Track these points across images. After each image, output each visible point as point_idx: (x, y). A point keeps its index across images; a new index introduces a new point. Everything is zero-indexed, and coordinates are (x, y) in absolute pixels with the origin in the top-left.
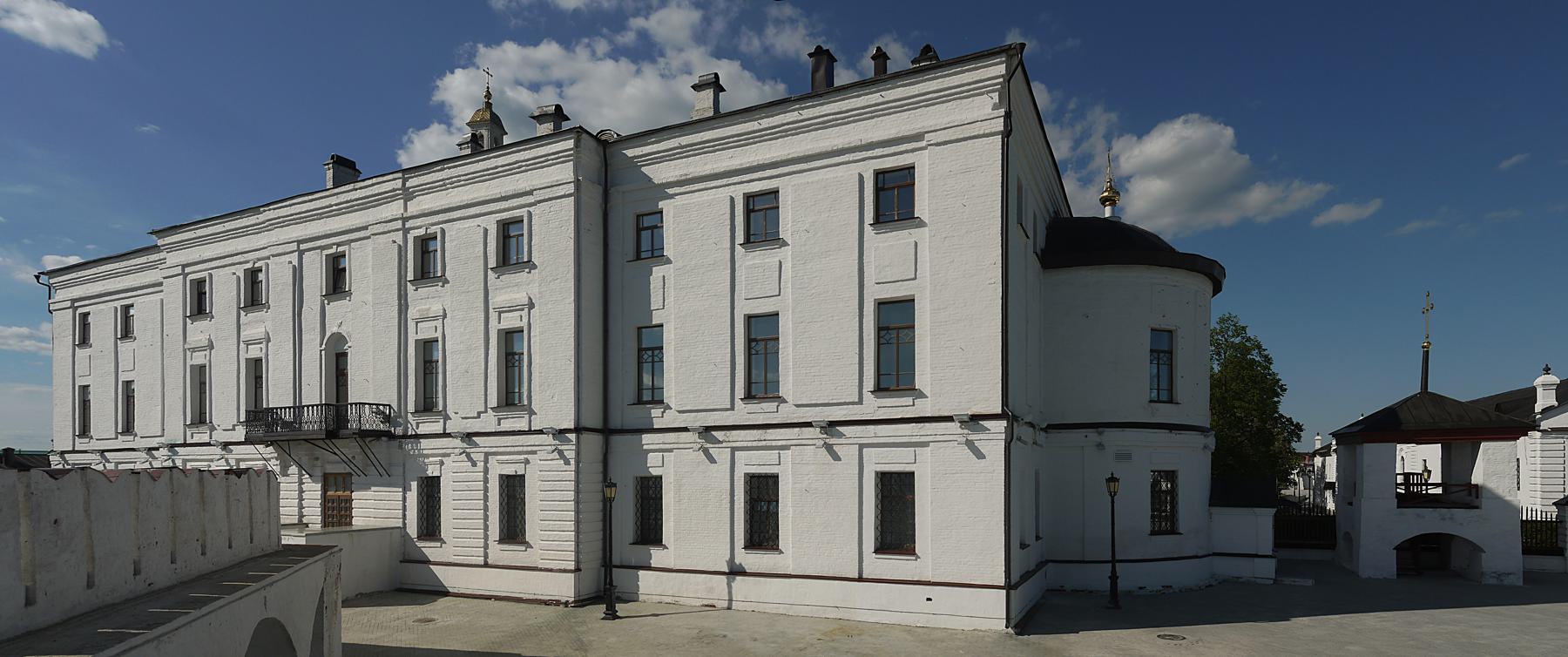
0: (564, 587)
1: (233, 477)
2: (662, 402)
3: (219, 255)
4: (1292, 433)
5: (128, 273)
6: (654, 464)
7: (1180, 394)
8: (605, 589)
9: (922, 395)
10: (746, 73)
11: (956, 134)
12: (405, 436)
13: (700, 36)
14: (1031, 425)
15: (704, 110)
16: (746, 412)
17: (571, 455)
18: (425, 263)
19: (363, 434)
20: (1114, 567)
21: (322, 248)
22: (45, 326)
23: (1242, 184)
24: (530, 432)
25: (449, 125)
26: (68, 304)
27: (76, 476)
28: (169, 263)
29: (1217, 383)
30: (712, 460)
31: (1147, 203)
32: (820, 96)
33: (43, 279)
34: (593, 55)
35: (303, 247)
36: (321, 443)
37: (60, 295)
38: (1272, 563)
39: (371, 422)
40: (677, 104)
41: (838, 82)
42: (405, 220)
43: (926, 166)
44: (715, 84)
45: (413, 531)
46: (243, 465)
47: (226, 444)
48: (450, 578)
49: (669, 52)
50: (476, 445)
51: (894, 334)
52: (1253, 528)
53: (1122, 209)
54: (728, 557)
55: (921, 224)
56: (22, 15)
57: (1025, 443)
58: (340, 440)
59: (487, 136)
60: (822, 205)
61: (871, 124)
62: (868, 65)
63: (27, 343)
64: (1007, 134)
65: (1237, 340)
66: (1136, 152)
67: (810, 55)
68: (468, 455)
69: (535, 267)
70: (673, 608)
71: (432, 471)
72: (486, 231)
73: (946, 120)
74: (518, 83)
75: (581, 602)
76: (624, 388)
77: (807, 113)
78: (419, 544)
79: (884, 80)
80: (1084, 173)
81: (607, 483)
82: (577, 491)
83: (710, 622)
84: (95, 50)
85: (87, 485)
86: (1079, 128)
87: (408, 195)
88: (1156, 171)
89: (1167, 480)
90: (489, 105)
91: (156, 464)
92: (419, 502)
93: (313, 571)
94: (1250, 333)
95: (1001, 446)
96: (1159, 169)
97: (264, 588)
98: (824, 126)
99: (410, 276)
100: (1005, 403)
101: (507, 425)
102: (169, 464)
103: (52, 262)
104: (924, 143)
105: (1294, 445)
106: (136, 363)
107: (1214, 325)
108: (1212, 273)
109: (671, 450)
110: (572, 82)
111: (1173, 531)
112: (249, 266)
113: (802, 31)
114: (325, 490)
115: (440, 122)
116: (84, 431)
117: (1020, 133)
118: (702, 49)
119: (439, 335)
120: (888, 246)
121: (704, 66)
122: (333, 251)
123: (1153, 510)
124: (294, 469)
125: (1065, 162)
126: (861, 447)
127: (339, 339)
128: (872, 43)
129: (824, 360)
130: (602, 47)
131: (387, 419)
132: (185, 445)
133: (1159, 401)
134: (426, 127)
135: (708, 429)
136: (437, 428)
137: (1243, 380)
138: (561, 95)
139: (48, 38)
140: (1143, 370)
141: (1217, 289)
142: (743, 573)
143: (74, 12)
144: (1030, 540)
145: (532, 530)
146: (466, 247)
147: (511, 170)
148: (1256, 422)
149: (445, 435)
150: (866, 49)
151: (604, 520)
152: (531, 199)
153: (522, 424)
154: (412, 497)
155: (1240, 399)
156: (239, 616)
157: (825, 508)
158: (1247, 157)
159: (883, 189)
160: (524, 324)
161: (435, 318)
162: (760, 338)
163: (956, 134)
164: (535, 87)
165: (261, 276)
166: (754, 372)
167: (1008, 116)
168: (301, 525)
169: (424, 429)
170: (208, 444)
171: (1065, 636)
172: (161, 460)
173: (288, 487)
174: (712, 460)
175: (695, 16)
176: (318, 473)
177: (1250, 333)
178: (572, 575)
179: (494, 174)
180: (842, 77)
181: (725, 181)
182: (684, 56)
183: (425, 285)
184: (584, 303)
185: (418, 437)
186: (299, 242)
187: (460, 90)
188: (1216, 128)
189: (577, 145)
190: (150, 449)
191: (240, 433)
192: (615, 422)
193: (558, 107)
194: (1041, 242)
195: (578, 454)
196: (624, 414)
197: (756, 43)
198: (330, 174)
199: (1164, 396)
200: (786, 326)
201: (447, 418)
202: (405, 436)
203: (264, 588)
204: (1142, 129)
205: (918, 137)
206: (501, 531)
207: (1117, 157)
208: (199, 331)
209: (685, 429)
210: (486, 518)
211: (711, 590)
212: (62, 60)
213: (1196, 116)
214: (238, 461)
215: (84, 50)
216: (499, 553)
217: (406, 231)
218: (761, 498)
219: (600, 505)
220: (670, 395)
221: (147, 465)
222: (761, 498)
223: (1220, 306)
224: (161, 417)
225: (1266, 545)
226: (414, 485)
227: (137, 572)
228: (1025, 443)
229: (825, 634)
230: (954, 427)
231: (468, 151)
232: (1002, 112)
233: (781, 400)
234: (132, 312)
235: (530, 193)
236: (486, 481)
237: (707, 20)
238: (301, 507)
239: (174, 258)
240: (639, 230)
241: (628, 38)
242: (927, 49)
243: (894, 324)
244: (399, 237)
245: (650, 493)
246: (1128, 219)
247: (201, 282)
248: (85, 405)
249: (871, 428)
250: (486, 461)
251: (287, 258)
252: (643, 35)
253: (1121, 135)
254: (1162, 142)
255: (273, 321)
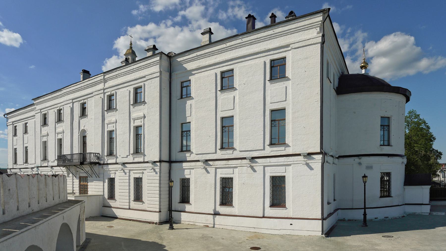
0: (155, 218)
1: (54, 177)
2: (190, 151)
3: (49, 105)
4: (437, 156)
5: (26, 113)
6: (187, 174)
7: (392, 142)
8: (170, 220)
9: (288, 146)
10: (221, 27)
11: (302, 47)
12: (104, 164)
13: (204, 15)
14: (332, 156)
15: (206, 42)
16: (221, 154)
17: (158, 170)
18: (110, 104)
19: (91, 163)
20: (365, 211)
21: (79, 101)
22: (6, 130)
23: (418, 59)
24: (144, 162)
25: (118, 56)
26: (11, 123)
27: (13, 176)
28: (37, 109)
29: (407, 137)
30: (208, 172)
31: (378, 68)
32: (250, 33)
33: (6, 116)
34: (167, 27)
35: (74, 101)
36: (78, 166)
37: (10, 120)
38: (429, 207)
39: (94, 160)
40: (196, 40)
41: (256, 27)
42: (104, 89)
43: (290, 56)
44: (210, 32)
45: (106, 196)
46: (57, 173)
47: (52, 167)
48: (118, 213)
49: (193, 22)
50: (126, 167)
51: (277, 122)
52: (422, 193)
53: (369, 70)
54: (213, 208)
55: (288, 79)
56: (2, 37)
57: (329, 163)
58: (84, 164)
59: (131, 58)
60: (250, 73)
61: (268, 43)
62: (268, 20)
63: (2, 135)
64: (323, 43)
65: (416, 120)
66: (375, 47)
67: (246, 18)
68: (124, 171)
69: (146, 103)
70: (194, 226)
71: (112, 176)
72: (130, 92)
73: (298, 39)
74: (141, 39)
75: (161, 223)
76: (176, 146)
77: (245, 40)
78: (109, 201)
79: (274, 25)
80: (354, 56)
81: (170, 181)
82: (160, 184)
83: (206, 232)
84: (19, 44)
85: (17, 179)
86: (351, 39)
87: (105, 81)
88: (382, 55)
89: (387, 176)
90: (131, 47)
91: (34, 173)
92: (108, 187)
93: (76, 209)
94: (421, 117)
95: (320, 165)
96: (384, 54)
97: (63, 213)
98: (251, 44)
99: (106, 109)
100: (321, 147)
101: (136, 160)
102: (37, 173)
103: (8, 110)
104: (290, 48)
105: (438, 160)
106: (24, 142)
107: (406, 114)
108: (406, 94)
109: (193, 169)
110: (159, 36)
111: (389, 196)
112: (58, 108)
113: (243, 9)
114: (80, 182)
115: (116, 55)
116: (15, 163)
117: (328, 41)
118: (205, 20)
119: (114, 129)
120: (275, 89)
121: (205, 25)
122: (82, 102)
123: (381, 188)
124: (71, 175)
125: (346, 53)
126: (264, 167)
127: (84, 131)
128: (270, 11)
129: (250, 134)
130: (169, 23)
131: (98, 158)
132: (41, 167)
133: (384, 145)
134: (111, 57)
135: (207, 161)
136: (113, 161)
137: (418, 136)
138: (155, 42)
139: (8, 43)
140: (378, 133)
141: (408, 100)
142: (219, 214)
143: (15, 34)
144: (332, 201)
145: (145, 197)
146: (123, 97)
147: (138, 69)
148: (423, 153)
149: (116, 163)
150: (267, 14)
151: (169, 194)
152: (145, 79)
153: (141, 160)
154: (106, 184)
155: (417, 143)
156: (55, 222)
157: (251, 190)
158: (420, 48)
159: (273, 67)
160: (142, 124)
161: (113, 123)
162: (226, 126)
163: (302, 47)
164: (146, 40)
165: (62, 111)
166: (224, 139)
167: (323, 36)
168: (73, 193)
169: (110, 161)
170: (47, 167)
171: (345, 237)
172: (35, 171)
173: (69, 180)
174: (208, 172)
175: (202, 8)
176: (78, 176)
177: (421, 117)
178: (158, 214)
179: (133, 71)
180: (258, 25)
181: (213, 67)
182: (198, 23)
183: (116, 114)
184: (163, 115)
185: (108, 164)
186: (73, 99)
187: (122, 44)
188: (407, 37)
189: (161, 59)
190: (32, 168)
191: (56, 163)
192: (173, 159)
193: (154, 46)
194: (336, 84)
195: (160, 170)
196: (176, 156)
197: (225, 15)
198: (82, 76)
199: (386, 143)
200: (236, 121)
201: (117, 158)
202: (104, 164)
203: (63, 213)
204: (377, 39)
205: (288, 46)
206: (134, 197)
207: (367, 50)
208: (45, 130)
209: (198, 161)
210: (129, 193)
211: (207, 220)
212: (12, 48)
213: (399, 33)
214: (55, 172)
215: (17, 45)
216: (134, 205)
217: (104, 93)
218: (226, 185)
219: (168, 189)
220: (193, 148)
221: (31, 173)
222: (226, 185)
223: (409, 107)
224: (35, 158)
225: (426, 199)
226: (107, 181)
227: (29, 206)
228: (329, 163)
229: (250, 237)
230: (301, 158)
231: (124, 64)
232: (321, 35)
233: (233, 149)
234: (27, 125)
235: (144, 77)
236: (129, 179)
237: (207, 9)
238: (73, 188)
239: (38, 107)
240: (182, 88)
241: (178, 19)
242: (291, 13)
243: (277, 118)
244: (102, 95)
245: (185, 185)
246: (371, 74)
247: (45, 115)
248: (16, 154)
249: (268, 159)
250: (129, 173)
251: (69, 105)
252: (184, 17)
253: (368, 42)
254: (385, 44)
255: (65, 126)
